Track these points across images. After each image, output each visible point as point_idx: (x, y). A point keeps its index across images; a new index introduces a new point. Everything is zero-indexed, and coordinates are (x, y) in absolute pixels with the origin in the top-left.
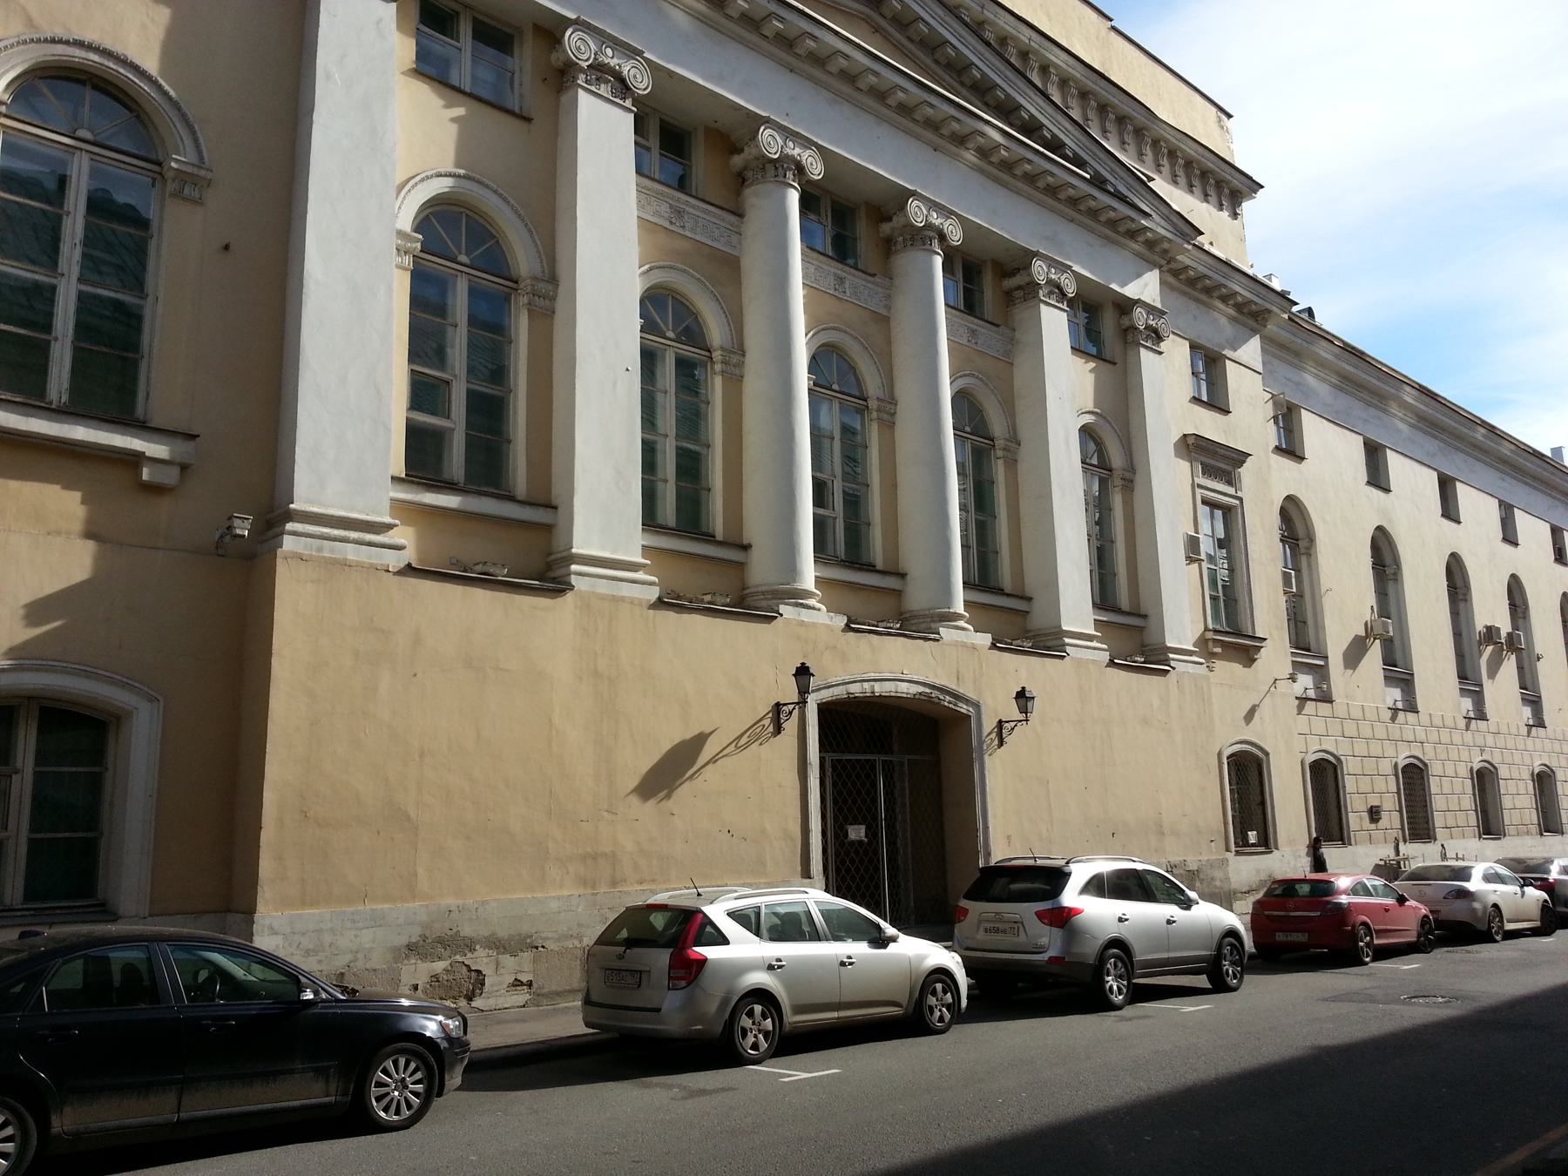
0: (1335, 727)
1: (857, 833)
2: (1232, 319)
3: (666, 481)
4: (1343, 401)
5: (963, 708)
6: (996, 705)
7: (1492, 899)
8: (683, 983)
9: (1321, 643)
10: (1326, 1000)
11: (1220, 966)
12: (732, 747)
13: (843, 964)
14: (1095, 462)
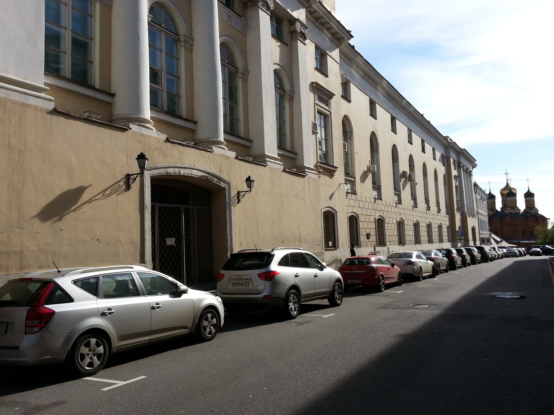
0: (357, 204)
1: (171, 241)
2: (330, 39)
3: (66, 53)
4: (364, 83)
5: (223, 185)
6: (237, 184)
7: (420, 265)
8: (37, 329)
9: (354, 172)
10: (381, 308)
11: (334, 295)
12: (101, 195)
13: (153, 308)
14: (278, 87)
